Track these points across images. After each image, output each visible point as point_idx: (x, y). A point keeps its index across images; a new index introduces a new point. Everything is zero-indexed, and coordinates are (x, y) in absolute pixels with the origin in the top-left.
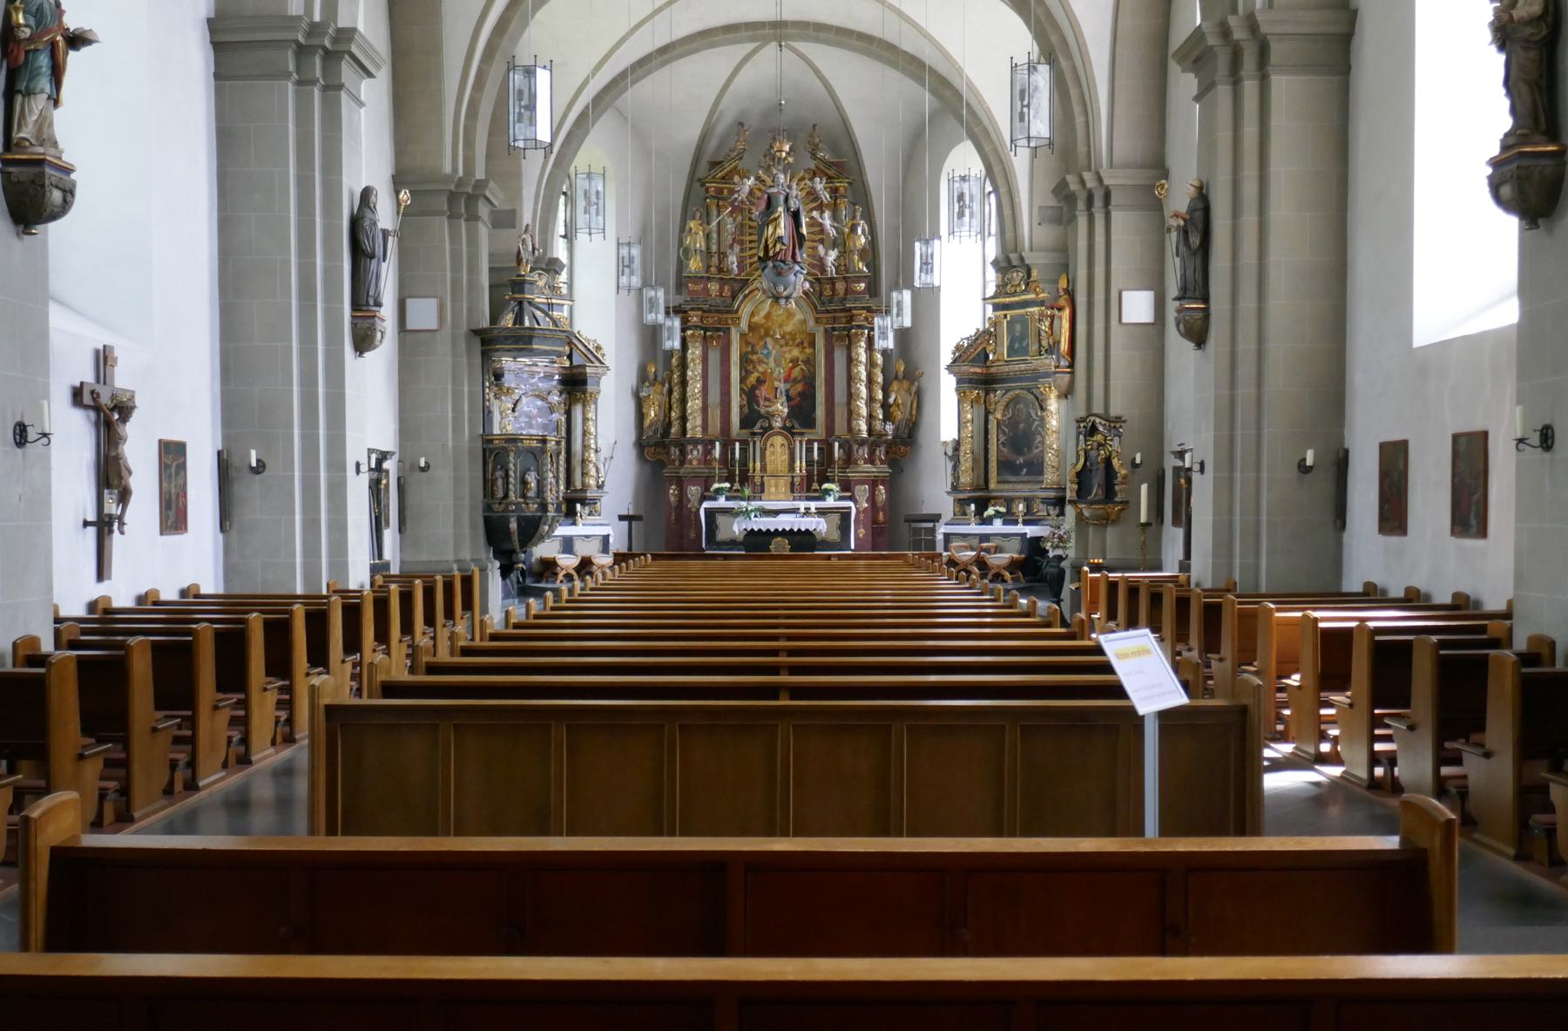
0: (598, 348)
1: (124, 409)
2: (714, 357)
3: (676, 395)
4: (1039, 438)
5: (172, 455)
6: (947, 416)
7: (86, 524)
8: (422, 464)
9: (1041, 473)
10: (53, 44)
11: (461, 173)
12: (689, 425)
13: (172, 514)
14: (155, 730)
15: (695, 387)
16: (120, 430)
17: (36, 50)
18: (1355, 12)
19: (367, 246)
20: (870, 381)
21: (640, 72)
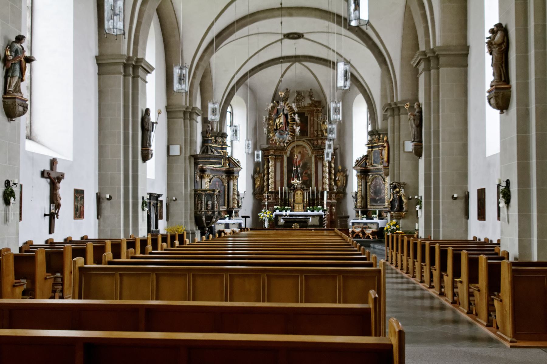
0: (239, 162)
1: (60, 177)
2: (278, 165)
3: (266, 177)
4: (383, 191)
5: (79, 194)
6: (354, 184)
7: (45, 215)
8: (174, 199)
9: (384, 203)
10: (21, 61)
11: (188, 105)
12: (270, 187)
13: (78, 213)
14: (46, 279)
15: (271, 174)
16: (58, 185)
17: (15, 63)
18: (469, 47)
19: (146, 127)
20: (330, 173)
21: (252, 73)
